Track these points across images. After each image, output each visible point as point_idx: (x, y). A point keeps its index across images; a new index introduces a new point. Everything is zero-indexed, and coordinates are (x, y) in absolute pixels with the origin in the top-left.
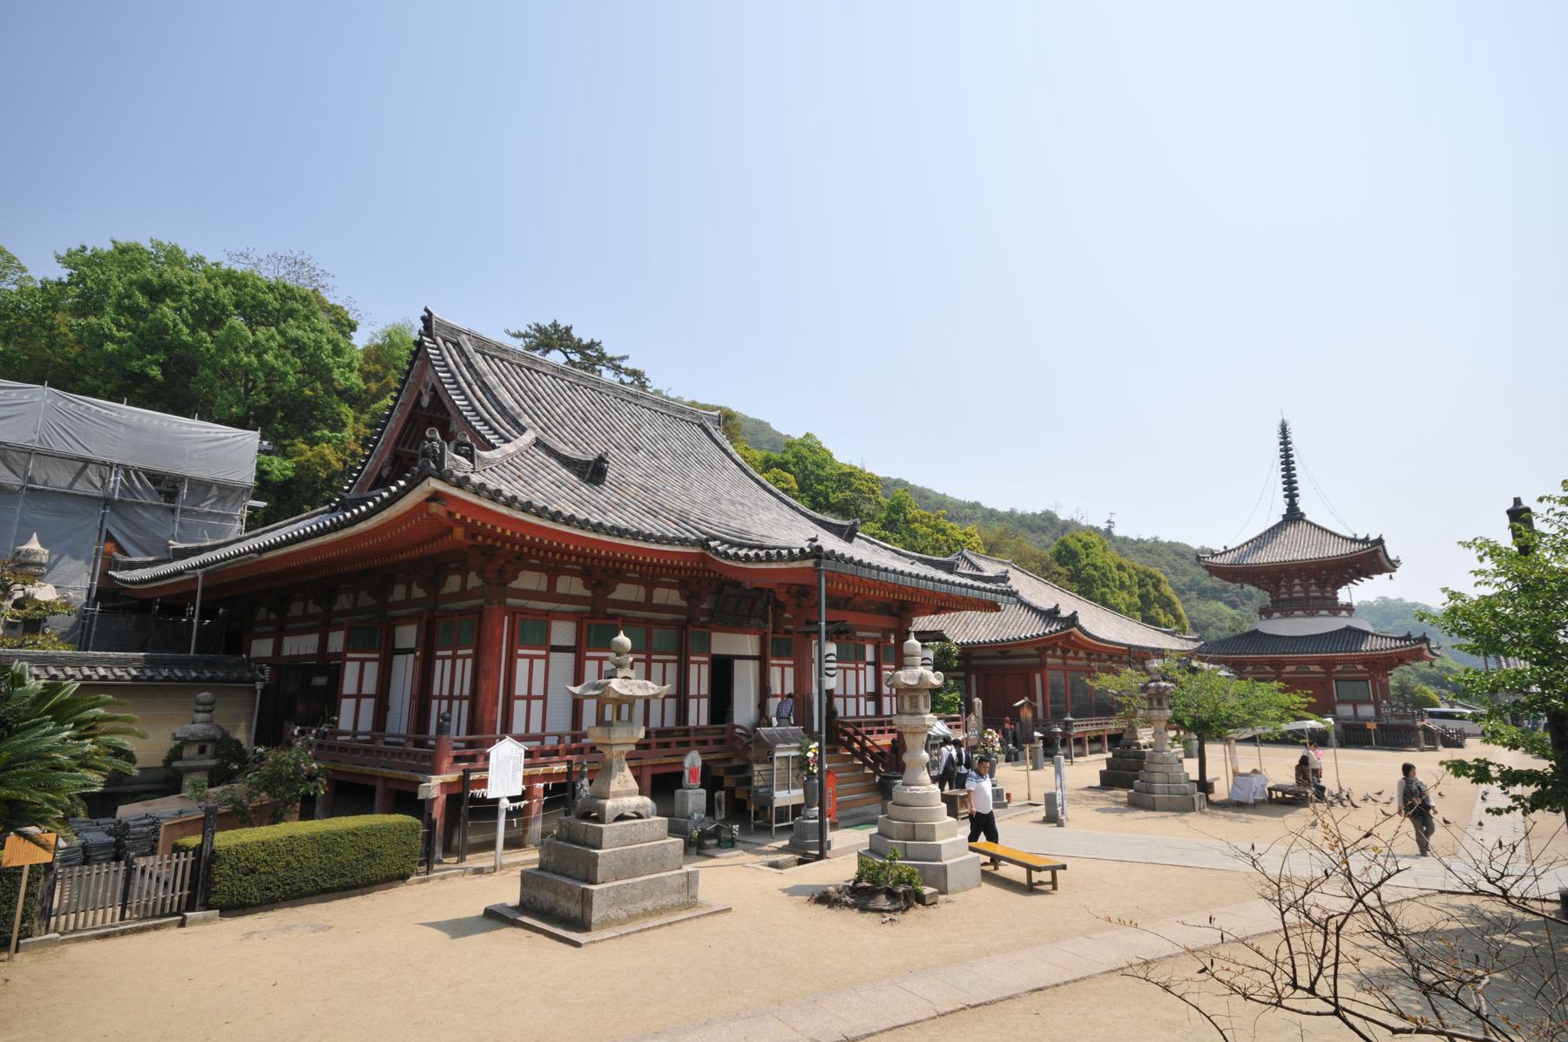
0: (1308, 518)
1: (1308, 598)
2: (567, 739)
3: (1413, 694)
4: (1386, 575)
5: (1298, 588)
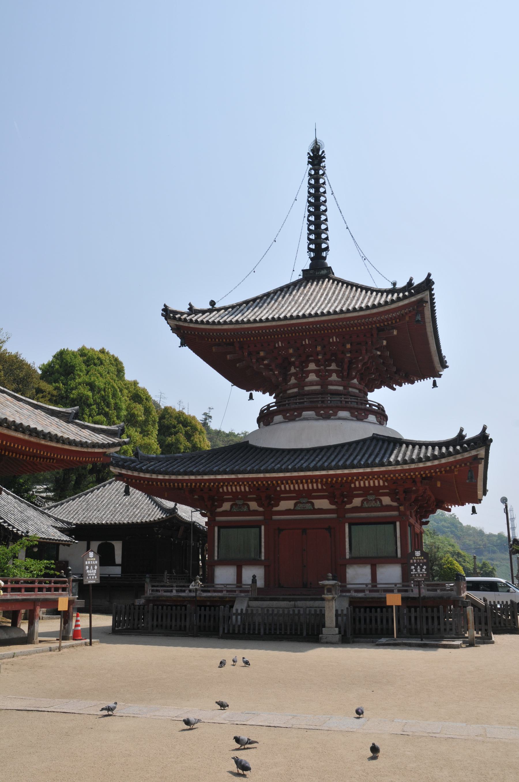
0: (338, 274)
1: (324, 392)
2: (370, 586)
3: (440, 566)
4: (429, 381)
5: (312, 377)
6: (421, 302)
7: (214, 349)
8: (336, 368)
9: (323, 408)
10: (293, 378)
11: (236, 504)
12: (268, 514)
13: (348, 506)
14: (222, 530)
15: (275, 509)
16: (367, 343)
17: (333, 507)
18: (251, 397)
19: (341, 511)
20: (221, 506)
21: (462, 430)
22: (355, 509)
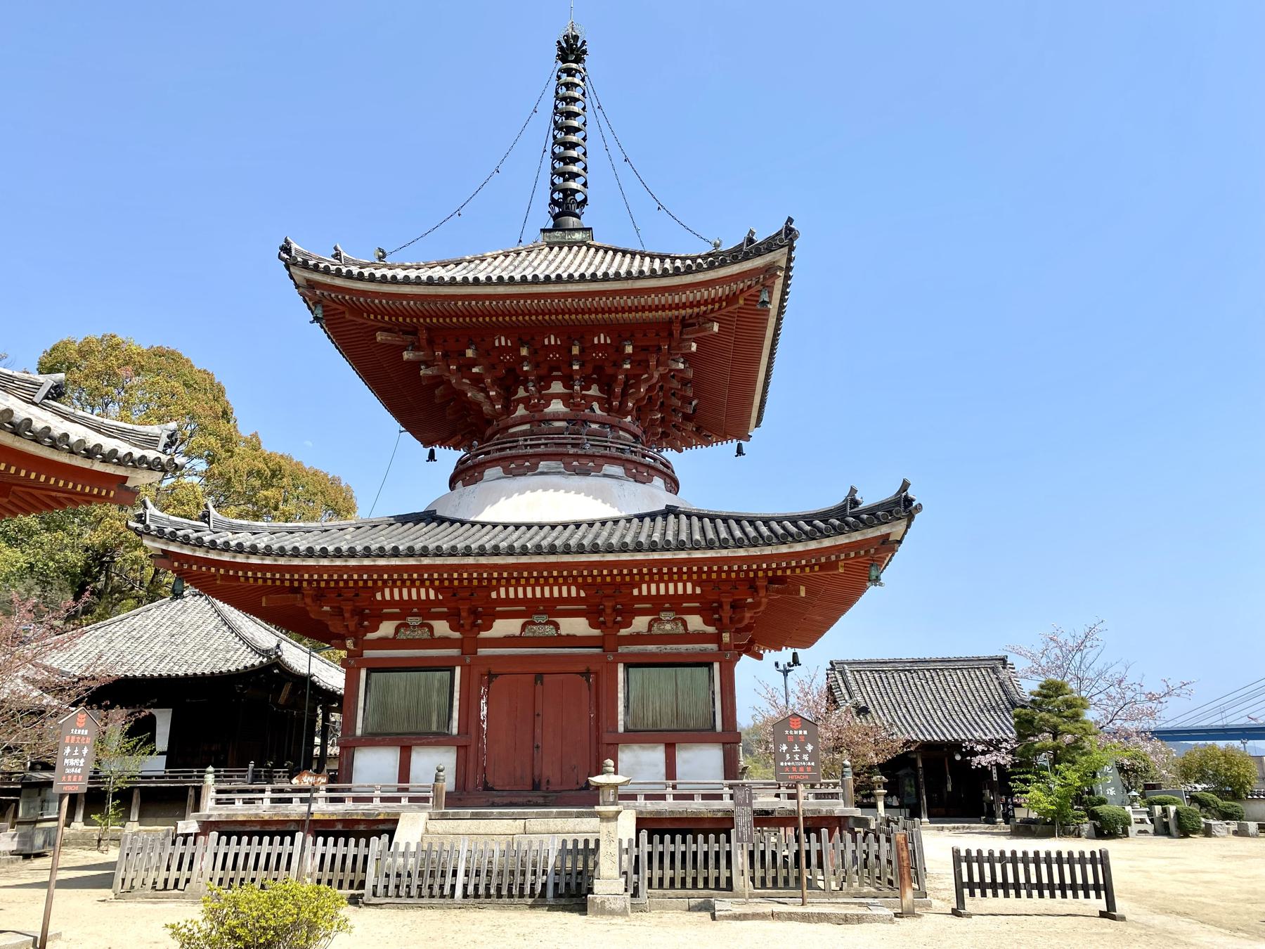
5: (557, 406)
6: (770, 270)
7: (380, 337)
8: (599, 394)
9: (576, 456)
10: (521, 406)
11: (406, 626)
12: (469, 645)
13: (623, 632)
14: (374, 675)
15: (483, 634)
16: (660, 349)
17: (597, 632)
18: (432, 457)
19: (607, 642)
20: (376, 629)
21: (853, 491)
22: (637, 639)
